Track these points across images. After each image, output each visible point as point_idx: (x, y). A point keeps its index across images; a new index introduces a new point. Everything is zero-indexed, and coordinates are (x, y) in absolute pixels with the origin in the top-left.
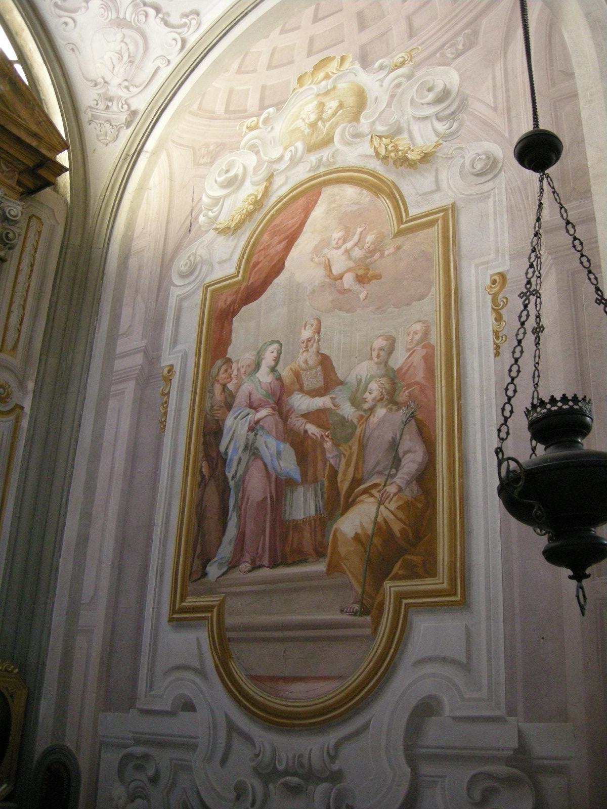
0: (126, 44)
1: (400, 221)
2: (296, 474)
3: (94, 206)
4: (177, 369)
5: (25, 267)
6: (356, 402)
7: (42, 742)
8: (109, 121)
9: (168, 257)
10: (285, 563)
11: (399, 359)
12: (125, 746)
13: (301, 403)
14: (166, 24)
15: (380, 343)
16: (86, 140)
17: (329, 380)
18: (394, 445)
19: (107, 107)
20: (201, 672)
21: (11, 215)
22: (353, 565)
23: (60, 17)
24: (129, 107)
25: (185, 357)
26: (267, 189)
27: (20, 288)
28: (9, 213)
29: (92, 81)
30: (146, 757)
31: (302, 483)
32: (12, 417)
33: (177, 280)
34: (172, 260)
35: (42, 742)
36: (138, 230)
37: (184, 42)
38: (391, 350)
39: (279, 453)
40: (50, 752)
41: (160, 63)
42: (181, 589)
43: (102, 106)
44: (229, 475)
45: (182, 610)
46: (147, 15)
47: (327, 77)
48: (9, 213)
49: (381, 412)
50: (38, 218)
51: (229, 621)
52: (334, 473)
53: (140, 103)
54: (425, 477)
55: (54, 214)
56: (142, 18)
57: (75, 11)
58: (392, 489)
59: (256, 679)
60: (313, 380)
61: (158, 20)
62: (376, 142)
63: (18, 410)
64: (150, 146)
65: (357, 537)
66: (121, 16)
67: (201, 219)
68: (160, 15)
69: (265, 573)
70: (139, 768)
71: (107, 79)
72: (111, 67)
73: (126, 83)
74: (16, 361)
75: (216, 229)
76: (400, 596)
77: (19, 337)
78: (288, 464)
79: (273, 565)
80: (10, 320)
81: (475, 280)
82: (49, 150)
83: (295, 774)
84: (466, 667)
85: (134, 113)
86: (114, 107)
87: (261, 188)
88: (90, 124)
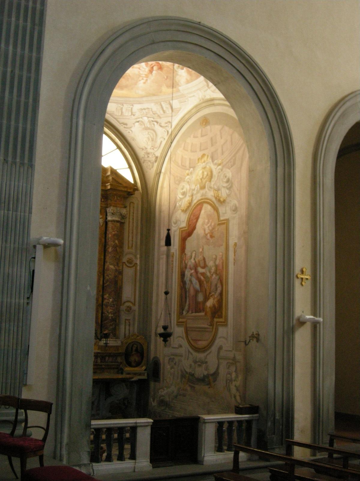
0: (150, 135)
1: (219, 221)
2: (199, 290)
3: (149, 192)
4: (175, 254)
5: (131, 220)
6: (210, 272)
7: (152, 356)
8: (150, 161)
9: (171, 212)
10: (121, 430)
11: (218, 262)
12: (169, 356)
13: (200, 270)
14: (161, 126)
15: (214, 257)
17: (205, 266)
18: (216, 285)
19: (148, 157)
20: (183, 338)
22: (209, 314)
23: (126, 131)
24: (155, 155)
25: (176, 251)
26: (192, 199)
27: (131, 228)
29: (141, 149)
30: (173, 359)
31: (201, 291)
32: (134, 267)
33: (173, 225)
34: (173, 214)
35: (152, 356)
36: (163, 203)
37: (168, 132)
38: (216, 259)
39: (196, 283)
40: (154, 358)
41: (162, 139)
42: (179, 318)
43: (146, 156)
44: (187, 287)
45: (179, 322)
46: (154, 124)
47: (204, 162)
49: (214, 276)
50: (133, 203)
51: (188, 325)
52: (206, 290)
53: (158, 154)
54: (221, 294)
56: (153, 125)
57: (131, 128)
58: (216, 296)
59: (192, 340)
60: (202, 264)
61: (158, 126)
62: (215, 191)
64: (163, 170)
65: (210, 308)
66: (146, 126)
67: (178, 204)
68: (158, 124)
69: (194, 314)
70: (172, 361)
71: (146, 147)
72: (146, 143)
73: (152, 148)
74: (133, 251)
75: (181, 210)
76: (217, 322)
78: (198, 286)
79: (195, 312)
81: (231, 243)
83: (199, 362)
84: (227, 339)
85: (157, 157)
86: (150, 156)
87: (190, 198)
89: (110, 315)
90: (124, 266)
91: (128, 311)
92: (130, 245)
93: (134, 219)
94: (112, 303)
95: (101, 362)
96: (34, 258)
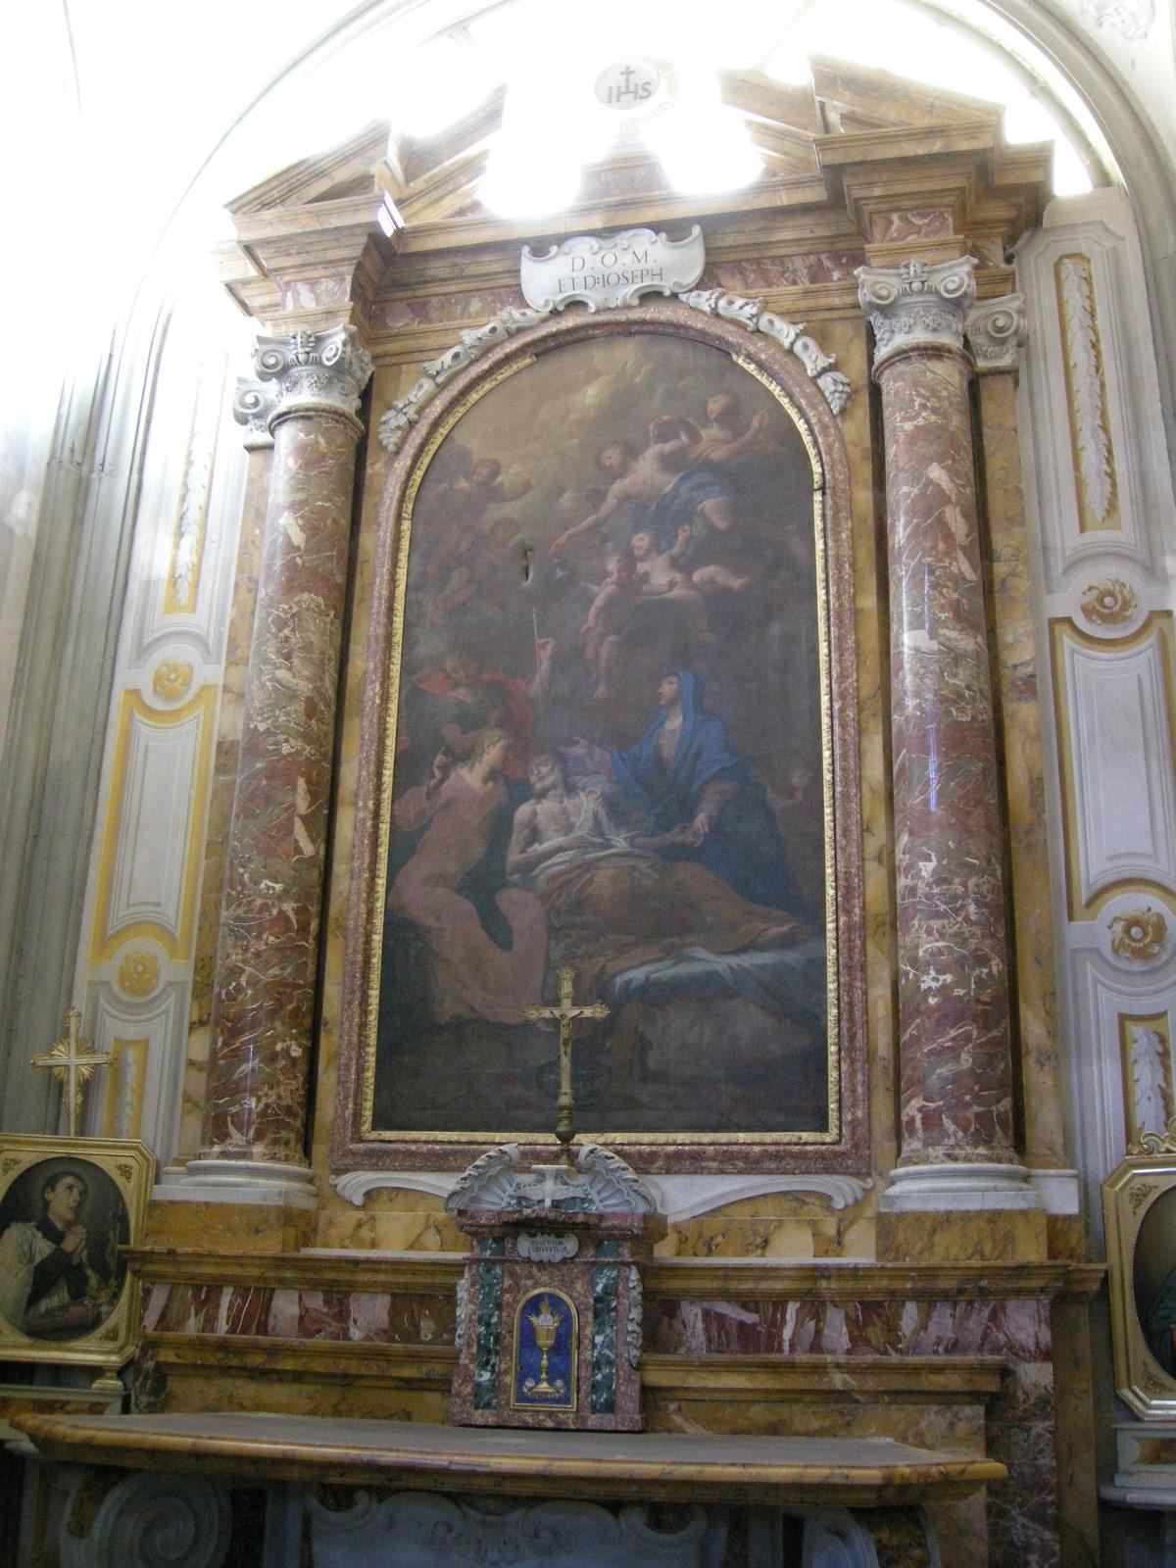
16: (1115, 62)
21: (955, 291)
27: (1084, 399)
28: (948, 291)
32: (1151, 640)
48: (948, 291)
50: (1078, 256)
55: (1107, 229)
63: (1158, 623)
77: (1114, 485)
80: (1083, 467)
82: (974, 137)
88: (1101, 25)
89: (928, 982)
90: (1067, 642)
91: (1141, 954)
92: (1096, 504)
93: (1104, 346)
94: (936, 890)
95: (858, 1340)
96: (1053, 994)
